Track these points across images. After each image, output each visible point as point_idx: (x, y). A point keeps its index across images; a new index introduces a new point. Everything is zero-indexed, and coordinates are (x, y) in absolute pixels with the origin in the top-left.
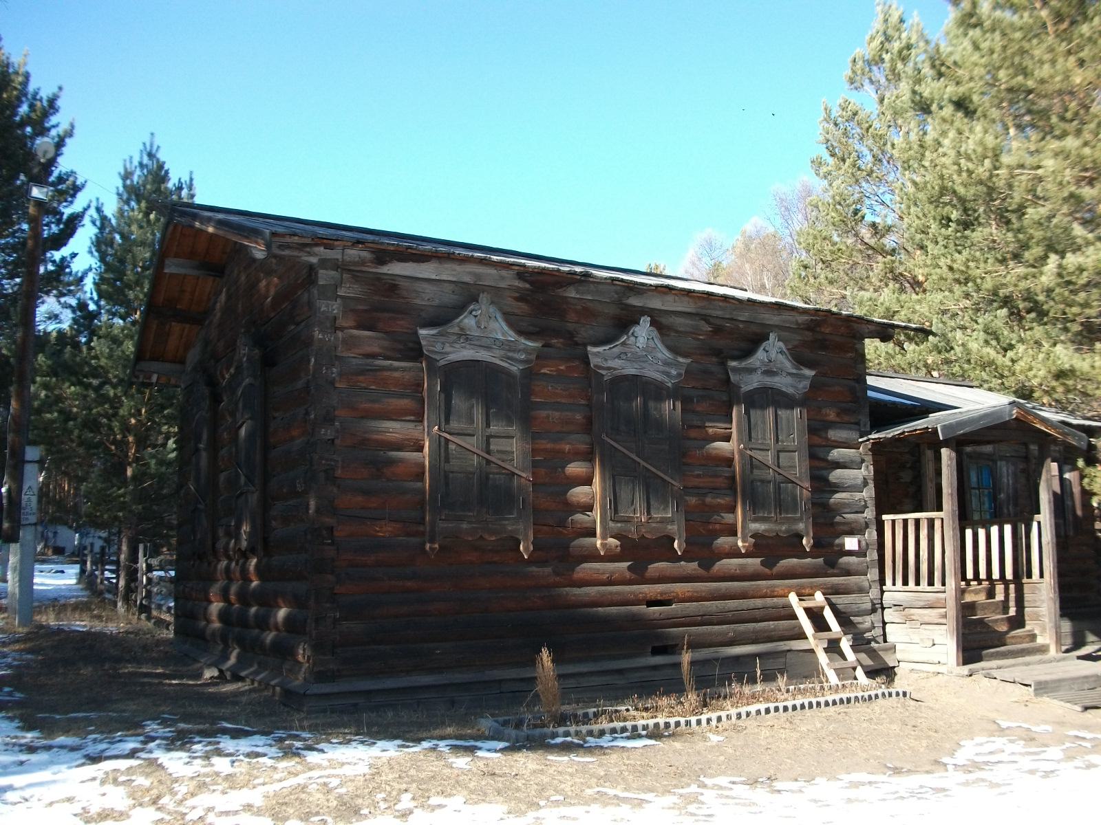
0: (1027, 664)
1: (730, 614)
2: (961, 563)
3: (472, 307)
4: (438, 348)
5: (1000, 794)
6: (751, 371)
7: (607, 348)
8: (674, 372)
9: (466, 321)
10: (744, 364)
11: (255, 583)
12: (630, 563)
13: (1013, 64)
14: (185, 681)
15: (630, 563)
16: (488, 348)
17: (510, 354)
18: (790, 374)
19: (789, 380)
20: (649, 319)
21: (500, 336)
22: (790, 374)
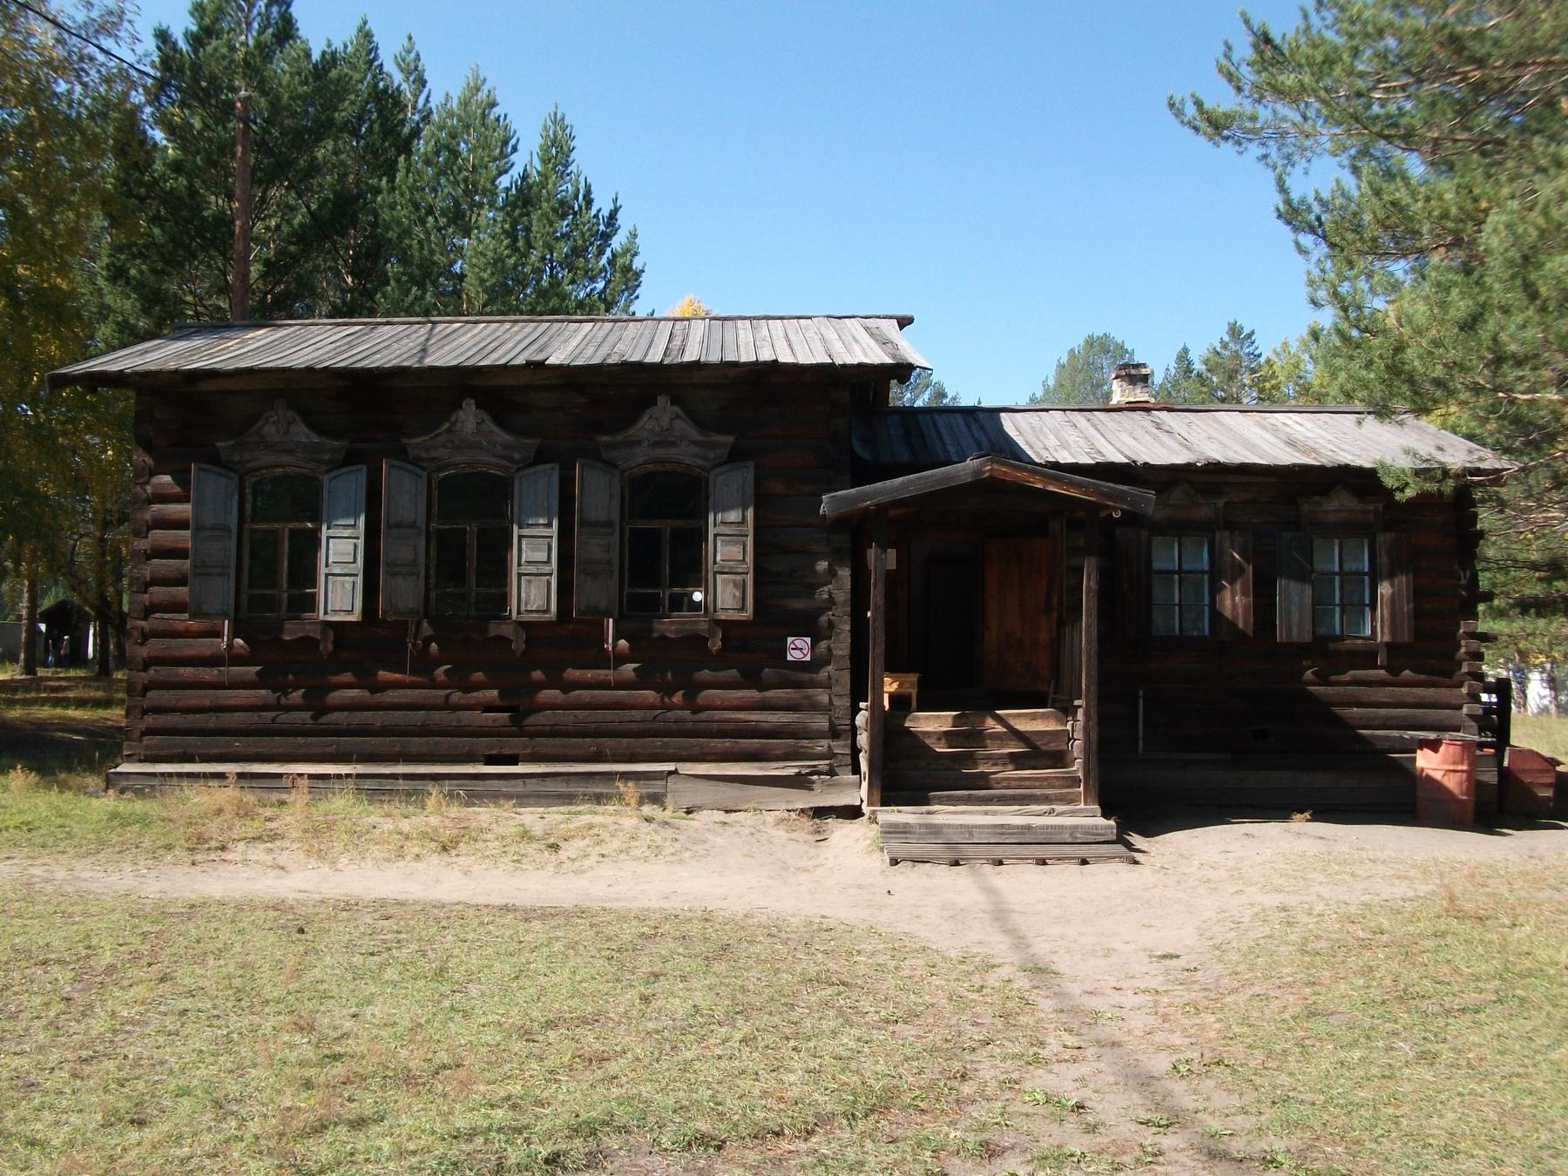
0: (899, 812)
1: (634, 726)
2: (181, 658)
3: (267, 414)
4: (236, 458)
5: (1172, 957)
6: (631, 444)
7: (426, 438)
8: (517, 456)
9: (266, 428)
10: (619, 437)
11: (890, 686)
12: (259, 668)
13: (1522, 146)
14: (1141, 742)
15: (259, 668)
16: (290, 452)
17: (316, 456)
18: (694, 443)
19: (693, 449)
20: (473, 401)
21: (304, 440)
22: (694, 443)
